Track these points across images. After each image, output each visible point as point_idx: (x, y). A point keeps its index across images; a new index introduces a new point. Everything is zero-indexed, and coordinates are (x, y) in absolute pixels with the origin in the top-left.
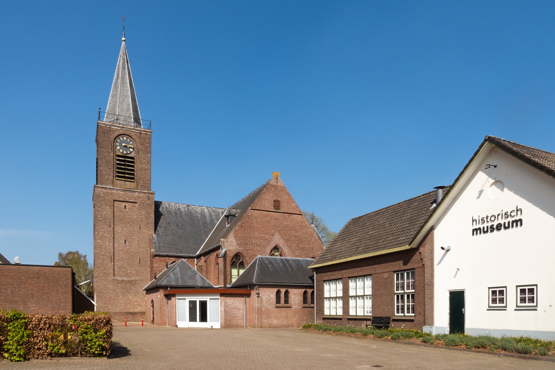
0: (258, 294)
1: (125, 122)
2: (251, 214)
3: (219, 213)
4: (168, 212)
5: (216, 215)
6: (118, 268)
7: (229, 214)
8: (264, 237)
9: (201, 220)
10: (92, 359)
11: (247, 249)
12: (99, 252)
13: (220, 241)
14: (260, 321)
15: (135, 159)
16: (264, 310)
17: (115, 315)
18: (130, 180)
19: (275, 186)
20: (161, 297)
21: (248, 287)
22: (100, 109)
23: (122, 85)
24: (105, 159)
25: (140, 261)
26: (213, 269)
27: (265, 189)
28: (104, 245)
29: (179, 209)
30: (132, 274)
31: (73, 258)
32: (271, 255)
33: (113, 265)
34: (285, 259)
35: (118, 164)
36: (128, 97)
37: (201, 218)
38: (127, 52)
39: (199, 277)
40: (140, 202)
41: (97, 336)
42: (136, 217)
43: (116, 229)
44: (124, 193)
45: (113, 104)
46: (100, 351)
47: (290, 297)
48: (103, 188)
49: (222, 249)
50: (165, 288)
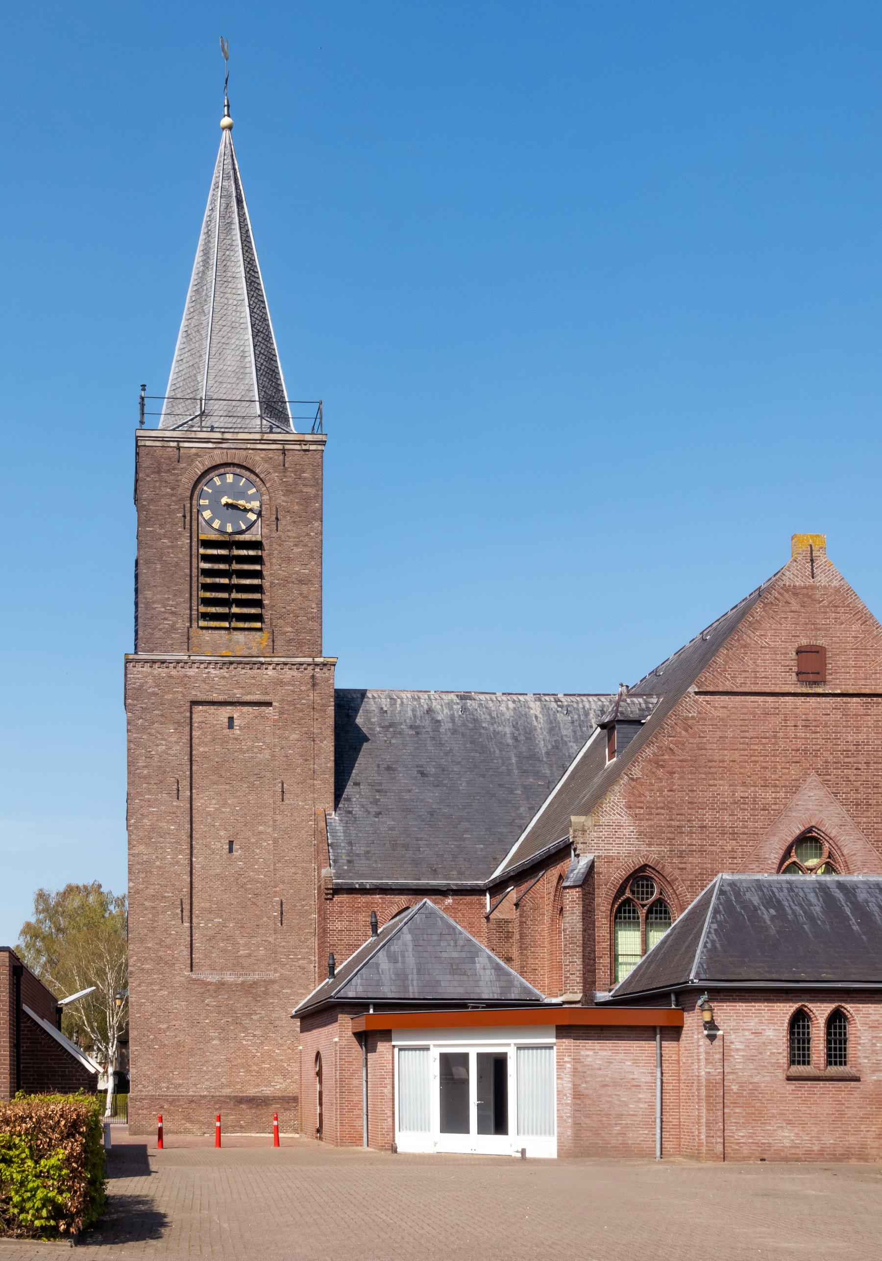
0: (711, 1025)
1: (230, 419)
2: (699, 713)
3: (587, 714)
4: (386, 728)
5: (577, 724)
6: (205, 939)
7: (616, 715)
8: (755, 797)
9: (515, 747)
10: (26, 1243)
11: (681, 852)
12: (141, 886)
13: (570, 824)
14: (720, 1134)
15: (266, 547)
16: (735, 1088)
17: (193, 1105)
18: (247, 625)
19: (805, 591)
20: (344, 1042)
21: (673, 998)
22: (144, 387)
23: (221, 290)
24: (160, 559)
25: (282, 913)
26: (546, 933)
27: (758, 609)
28: (158, 863)
29: (430, 711)
30: (252, 960)
31: (82, 907)
32: (787, 871)
33: (188, 932)
34: (840, 885)
35: (206, 573)
36: (243, 326)
37: (516, 739)
38: (237, 167)
39: (488, 966)
40: (282, 701)
41: (41, 1172)
42: (267, 756)
43: (197, 804)
44: (227, 675)
45: (191, 363)
46: (47, 1219)
47: (851, 1038)
48: (154, 662)
49: (577, 856)
50: (356, 1007)
